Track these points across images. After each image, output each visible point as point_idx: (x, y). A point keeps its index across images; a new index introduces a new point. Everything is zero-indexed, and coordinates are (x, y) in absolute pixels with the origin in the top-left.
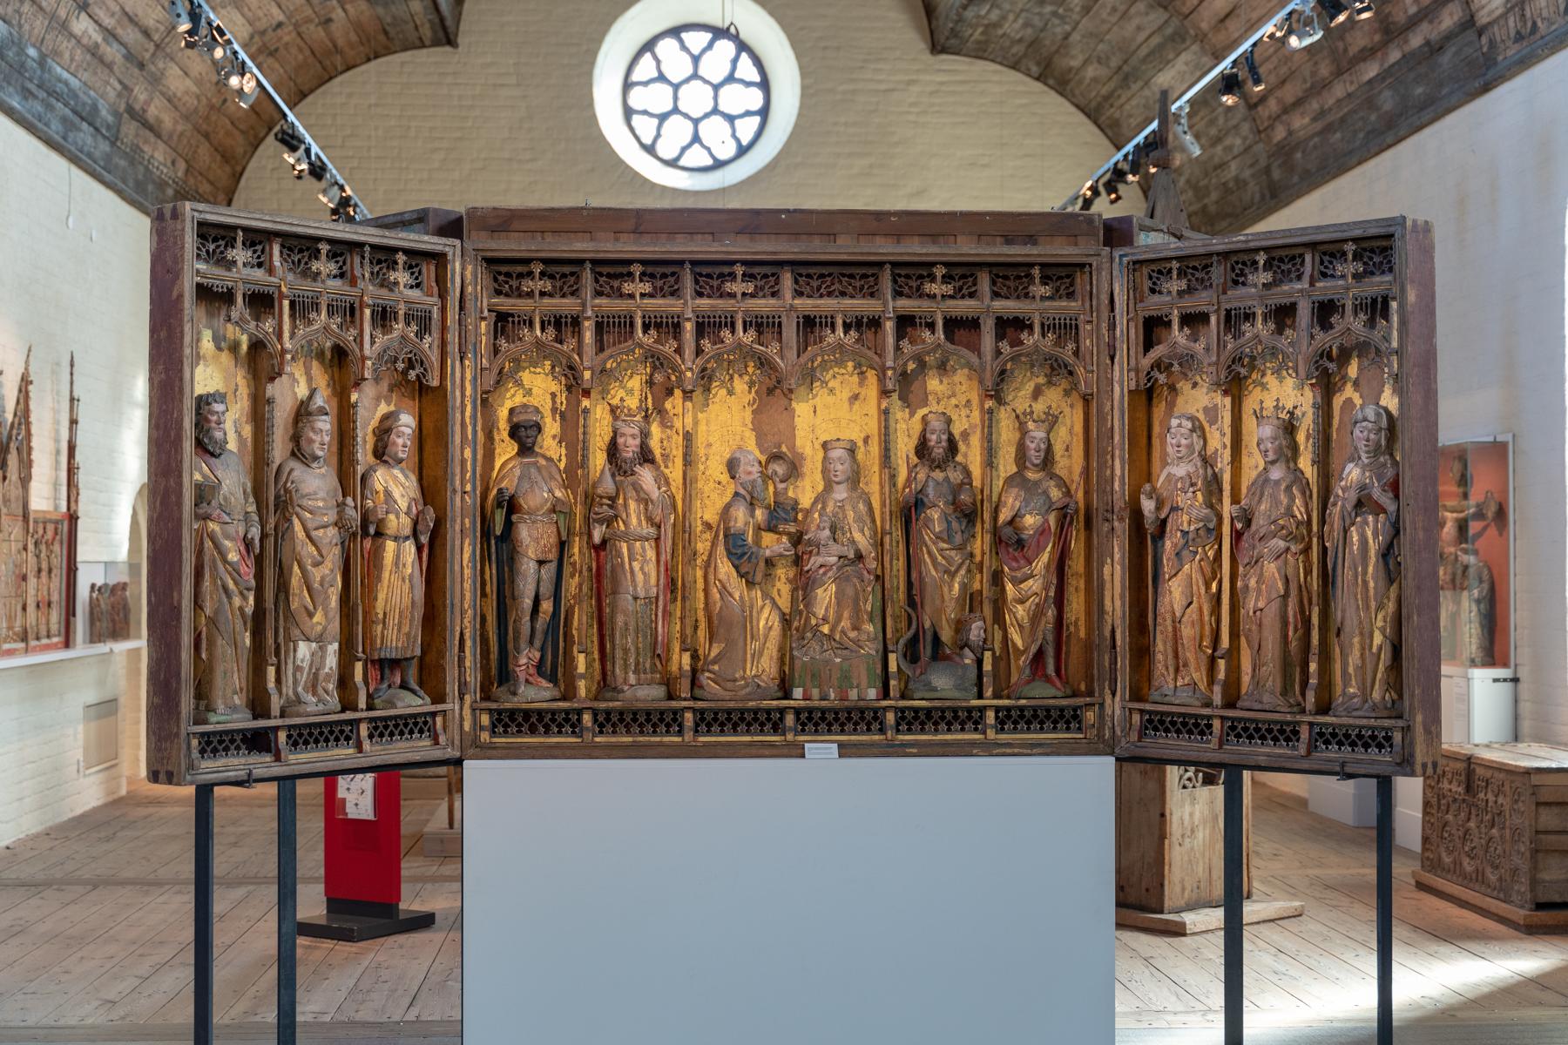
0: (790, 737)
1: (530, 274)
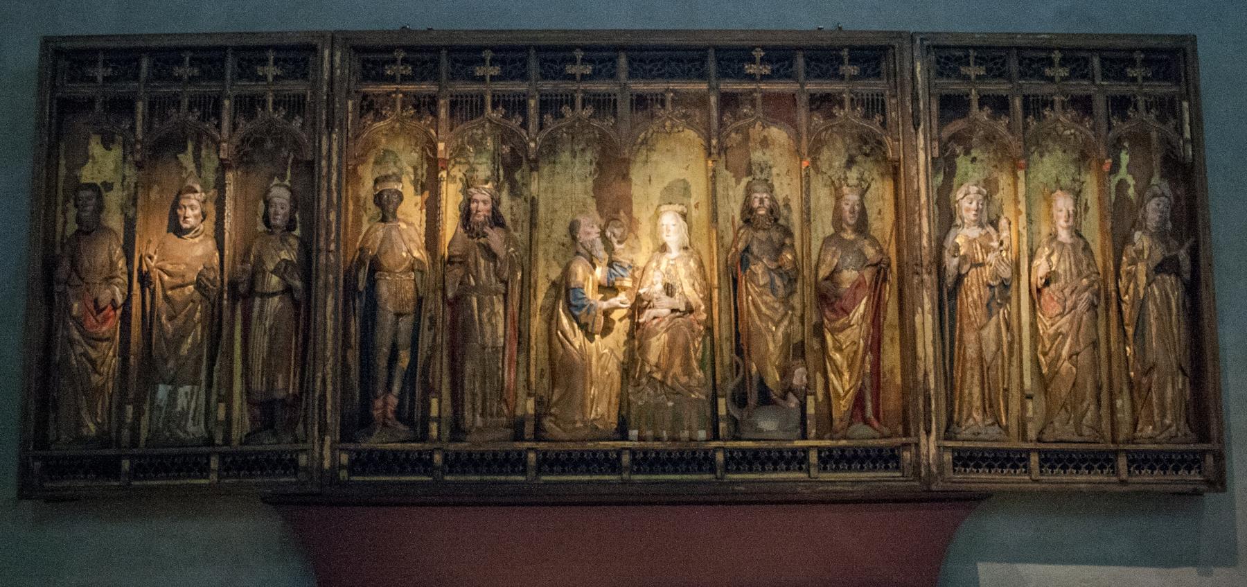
0: (625, 476)
1: (483, 61)
